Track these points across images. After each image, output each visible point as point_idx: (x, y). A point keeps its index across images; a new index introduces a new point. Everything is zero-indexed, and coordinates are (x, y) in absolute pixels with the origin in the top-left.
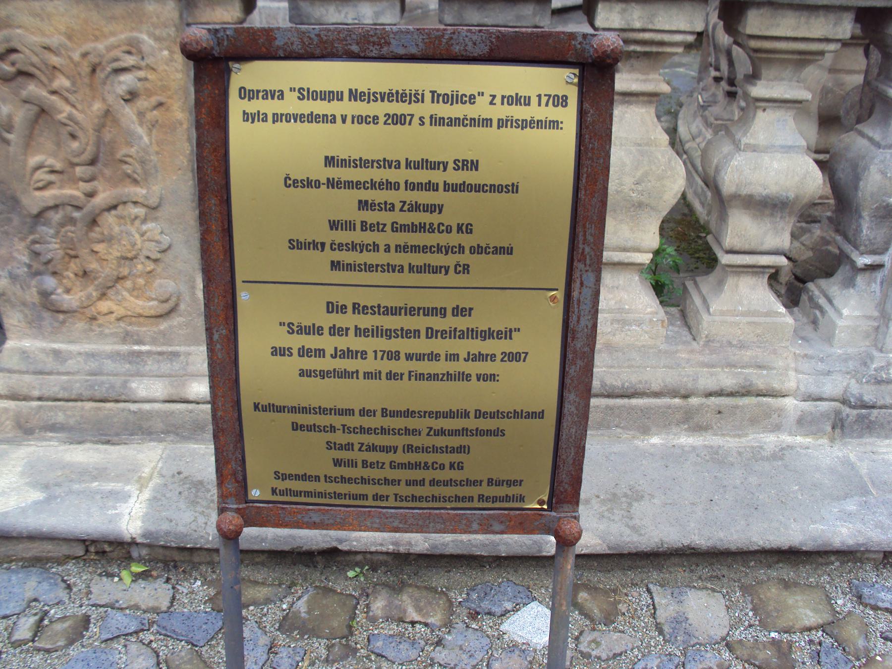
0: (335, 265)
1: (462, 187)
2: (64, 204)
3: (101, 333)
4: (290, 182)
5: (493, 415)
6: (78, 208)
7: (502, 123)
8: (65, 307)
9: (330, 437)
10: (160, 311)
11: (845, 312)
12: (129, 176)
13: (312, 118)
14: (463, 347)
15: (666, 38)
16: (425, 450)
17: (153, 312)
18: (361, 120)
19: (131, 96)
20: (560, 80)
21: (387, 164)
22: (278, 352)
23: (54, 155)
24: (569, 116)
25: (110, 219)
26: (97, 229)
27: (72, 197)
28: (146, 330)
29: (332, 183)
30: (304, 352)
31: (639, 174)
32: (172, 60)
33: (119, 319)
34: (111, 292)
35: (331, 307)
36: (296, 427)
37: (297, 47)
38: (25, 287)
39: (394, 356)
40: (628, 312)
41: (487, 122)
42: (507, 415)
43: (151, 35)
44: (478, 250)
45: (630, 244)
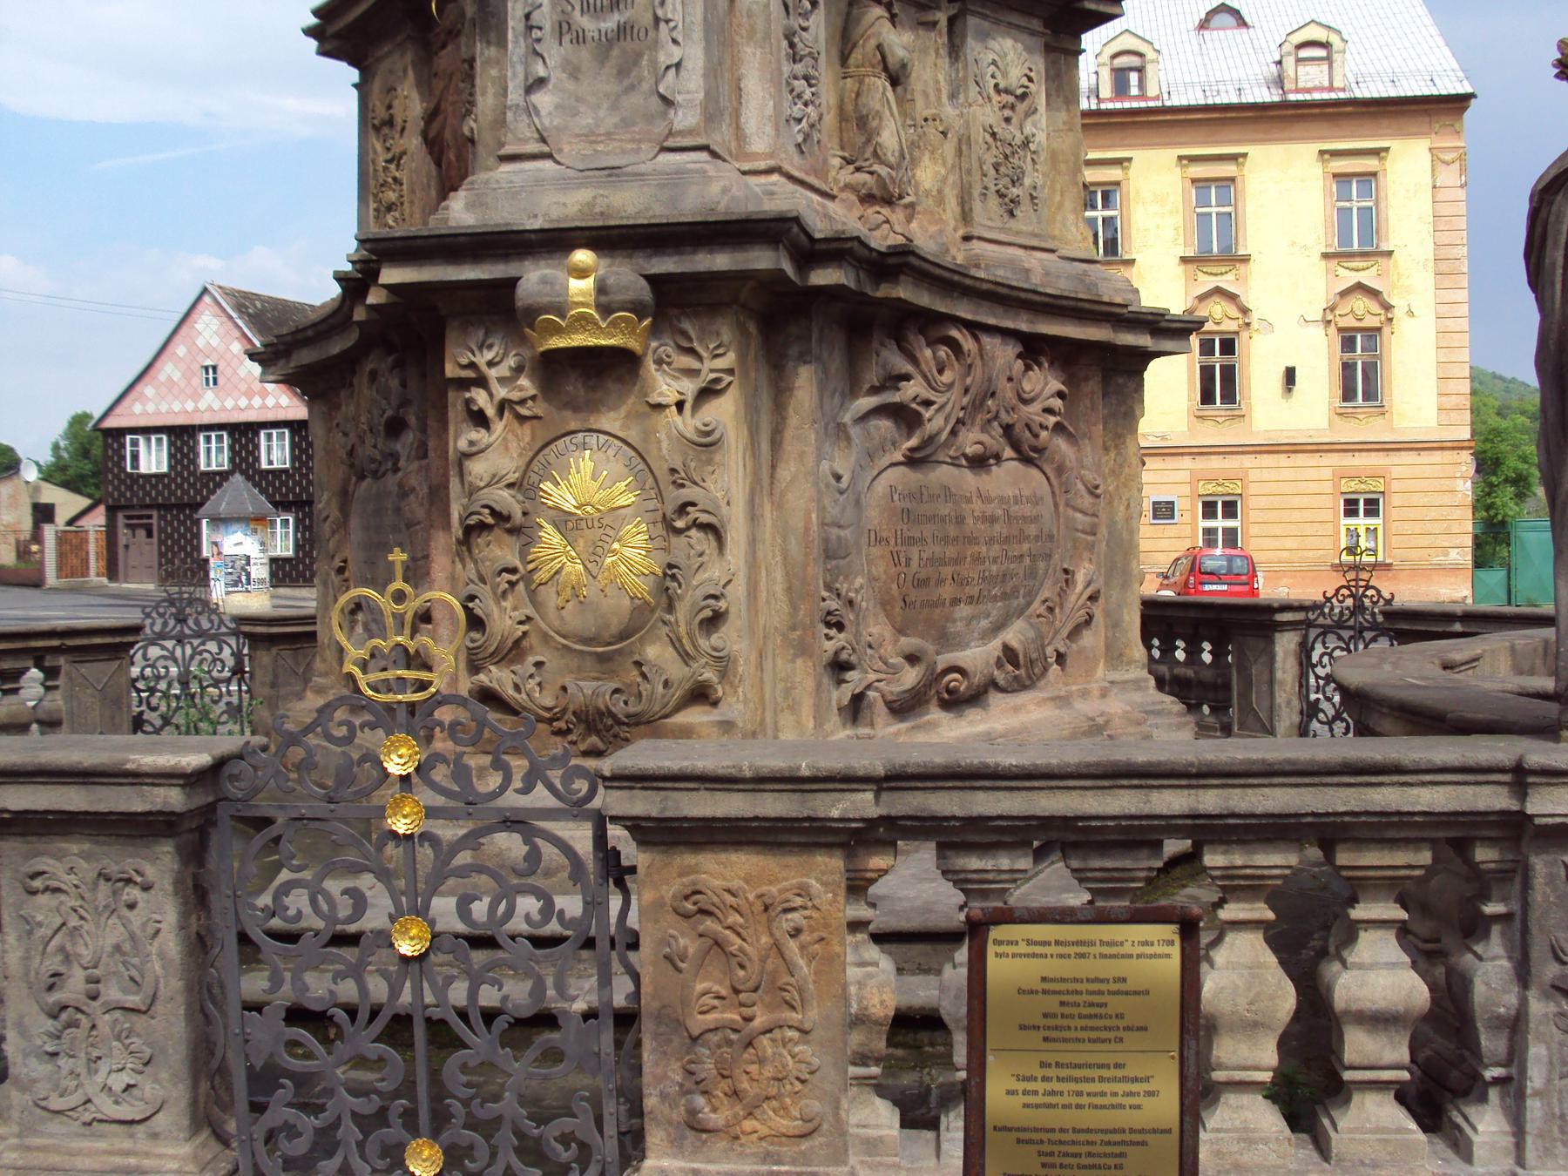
0: (1045, 1039)
1: (1118, 993)
2: (724, 1027)
3: (741, 1153)
4: (1021, 991)
5: (1141, 1131)
6: (735, 1031)
7: (1139, 956)
8: (711, 1125)
9: (1040, 1147)
10: (804, 1131)
11: (1480, 1128)
12: (787, 1003)
13: (1034, 955)
14: (1121, 1088)
15: (1266, 872)
16: (1099, 1155)
17: (797, 1132)
18: (1061, 956)
19: (796, 932)
20: (1169, 931)
21: (1076, 980)
22: (1010, 1092)
23: (720, 983)
24: (1175, 951)
25: (765, 1041)
26: (751, 1050)
27: (733, 1020)
28: (786, 1150)
29: (1045, 992)
30: (1025, 1092)
31: (1251, 995)
32: (835, 901)
33: (761, 1139)
34: (757, 1112)
35: (1043, 1065)
36: (1019, 1141)
37: (1026, 917)
38: (673, 1105)
39: (1079, 1094)
40: (1254, 1130)
41: (1131, 956)
42: (1148, 1132)
43: (817, 880)
44: (1128, 1029)
45: (1249, 1063)
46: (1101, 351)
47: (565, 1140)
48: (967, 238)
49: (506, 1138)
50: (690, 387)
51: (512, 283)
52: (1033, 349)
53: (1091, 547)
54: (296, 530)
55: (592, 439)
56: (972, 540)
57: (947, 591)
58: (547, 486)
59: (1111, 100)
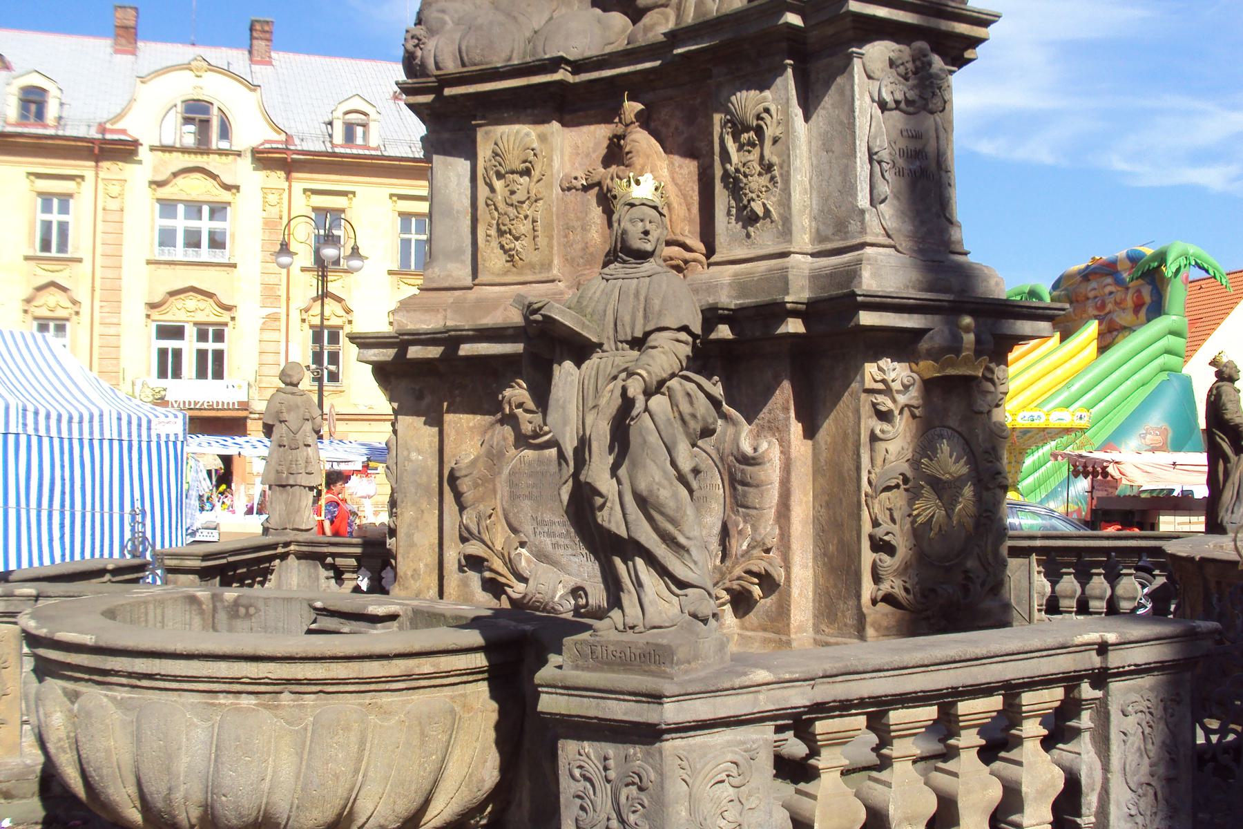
59: (18, 125)
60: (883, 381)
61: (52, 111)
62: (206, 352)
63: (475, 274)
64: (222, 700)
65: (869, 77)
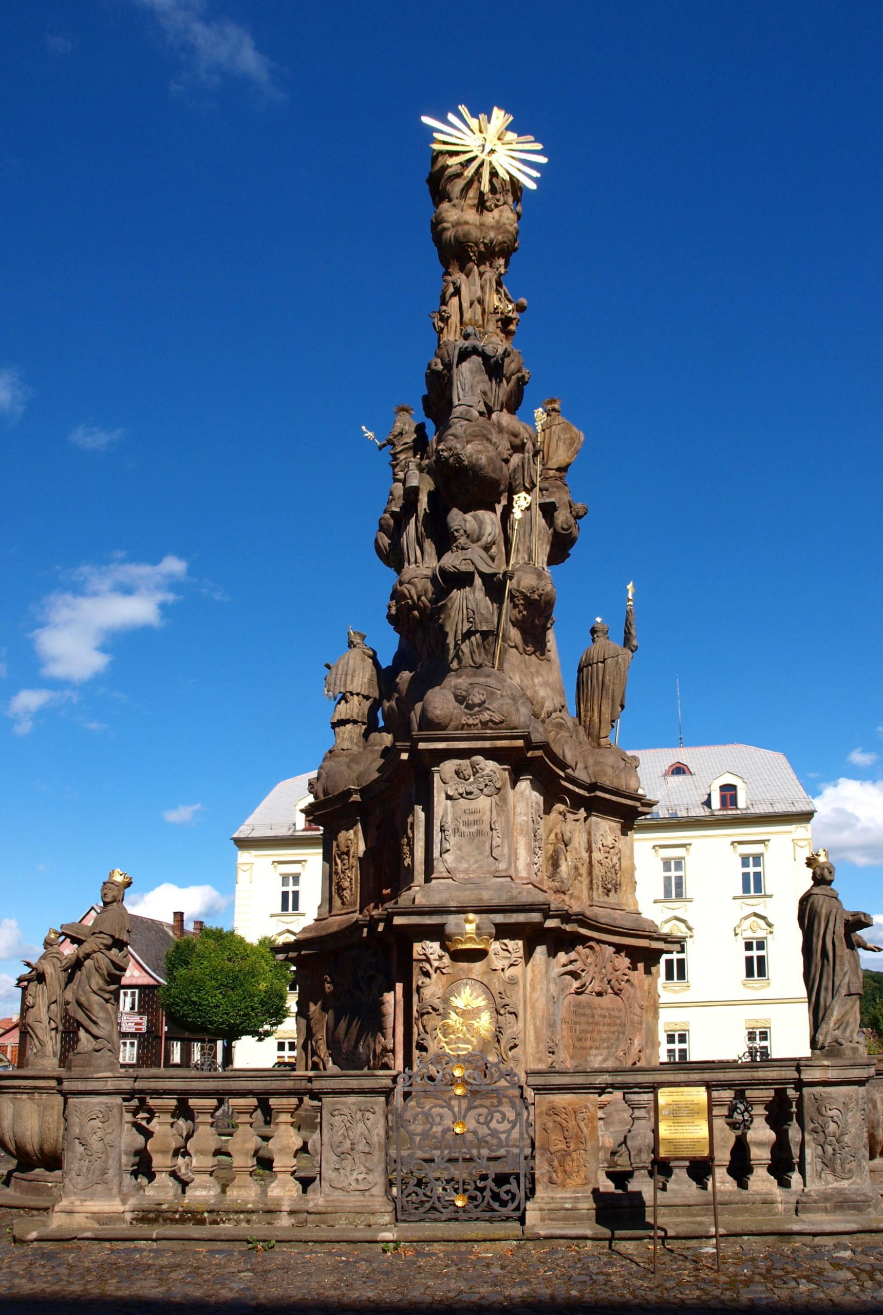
46: (649, 952)
47: (507, 1192)
48: (591, 906)
49: (487, 1193)
50: (506, 963)
51: (443, 925)
52: (619, 948)
53: (640, 1030)
54: (139, 1048)
55: (470, 982)
56: (597, 1024)
57: (588, 1044)
58: (452, 999)
59: (304, 830)
60: (425, 954)
61: (742, 802)
62: (752, 957)
63: (330, 911)
64: (19, 1096)
65: (444, 783)
